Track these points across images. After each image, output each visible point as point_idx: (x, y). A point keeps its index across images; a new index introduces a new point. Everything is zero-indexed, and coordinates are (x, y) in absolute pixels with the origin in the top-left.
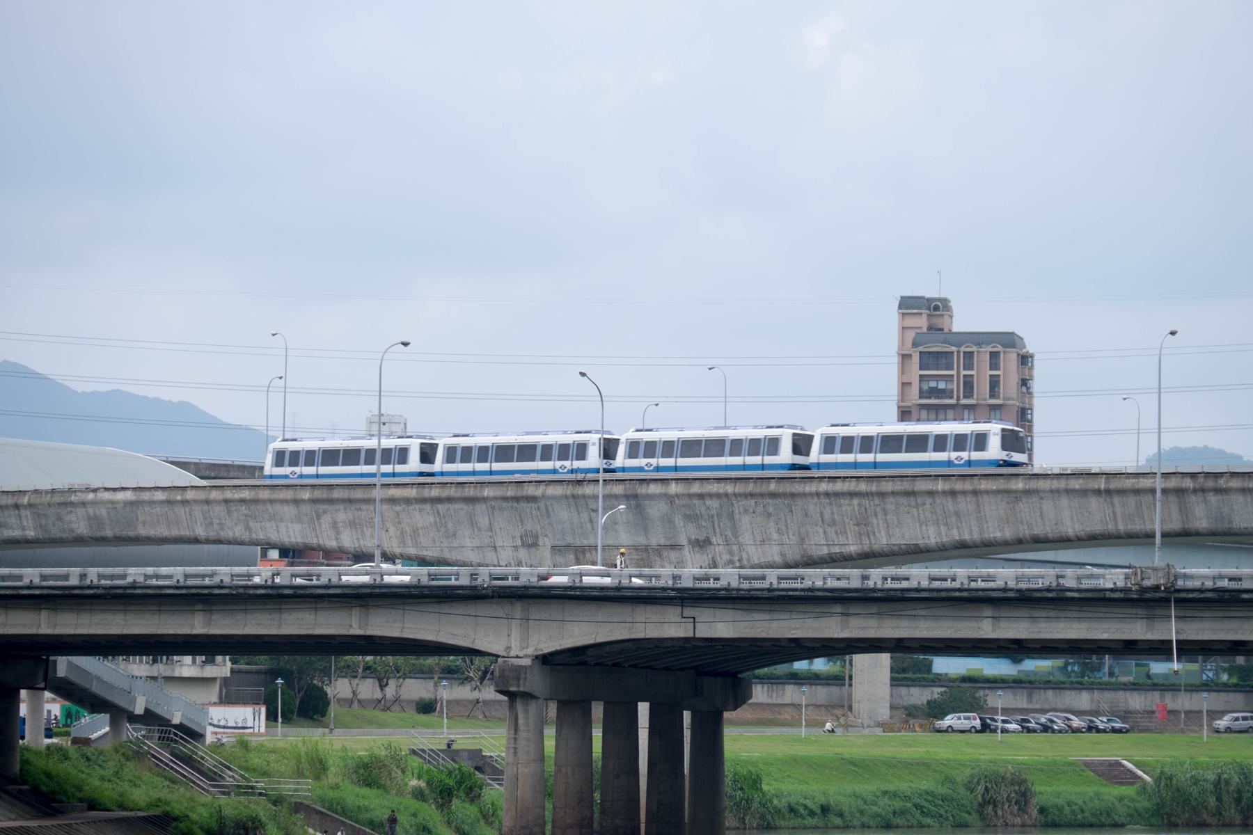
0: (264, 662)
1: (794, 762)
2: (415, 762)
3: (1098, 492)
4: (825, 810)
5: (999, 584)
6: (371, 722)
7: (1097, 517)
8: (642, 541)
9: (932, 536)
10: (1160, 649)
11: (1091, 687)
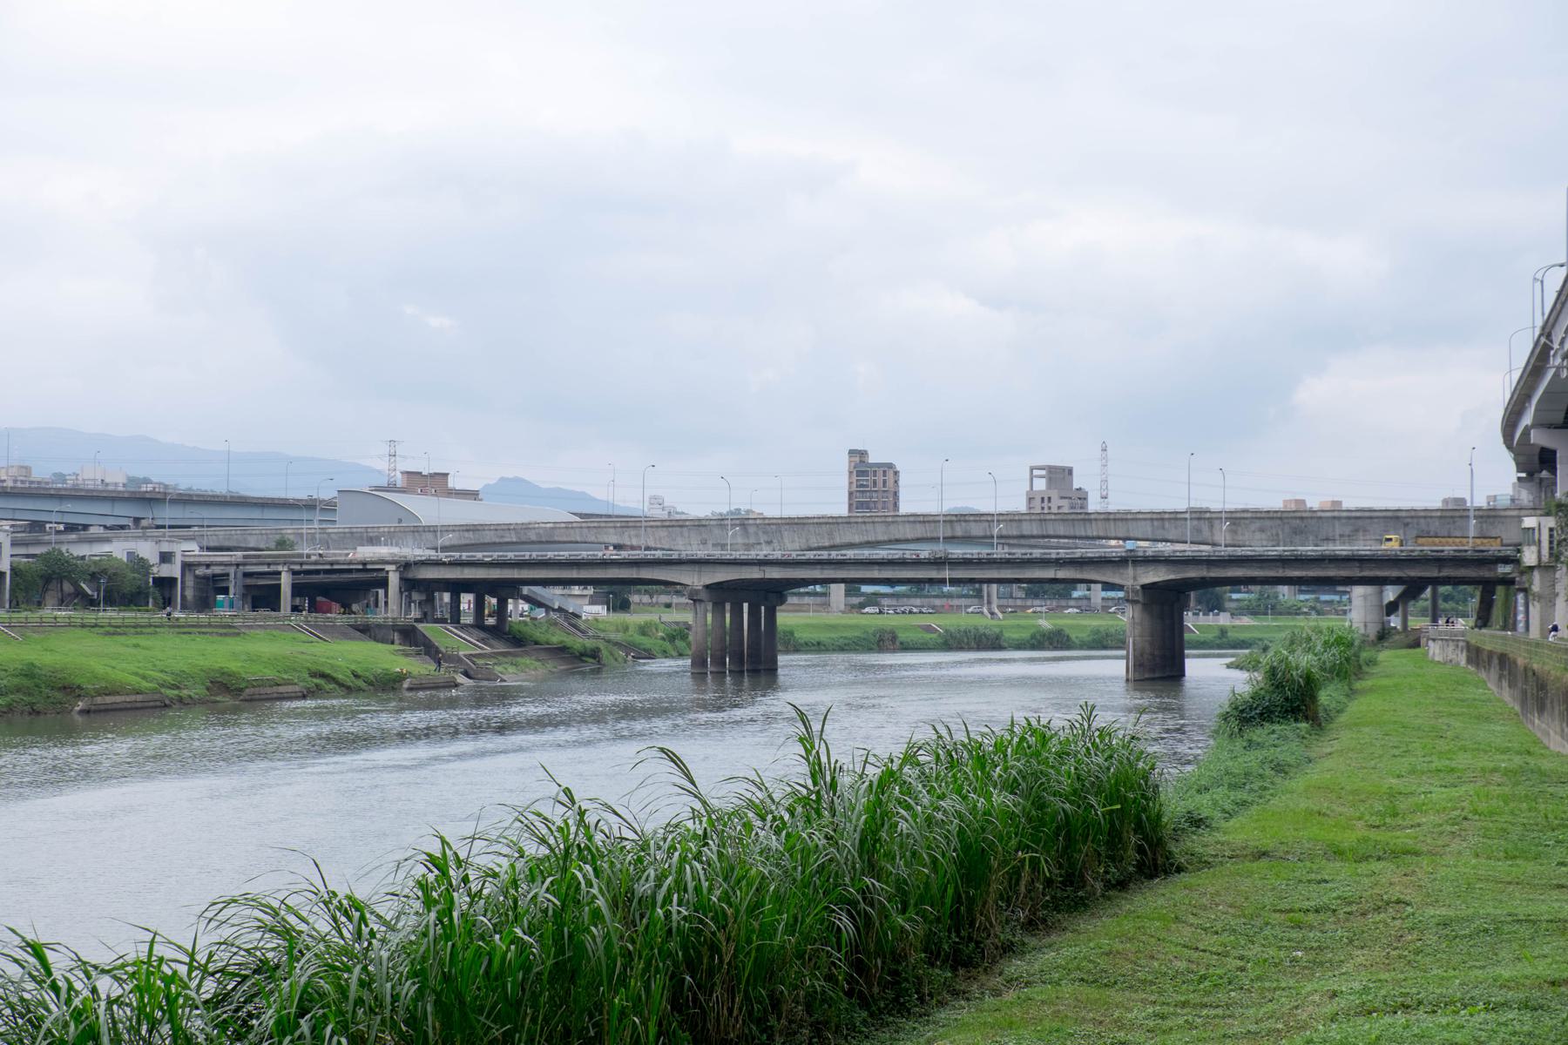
0: (606, 588)
1: (808, 626)
2: (662, 627)
3: (920, 522)
4: (819, 643)
5: (881, 557)
6: (647, 611)
7: (920, 531)
8: (746, 541)
9: (857, 539)
10: (942, 581)
11: (921, 597)
